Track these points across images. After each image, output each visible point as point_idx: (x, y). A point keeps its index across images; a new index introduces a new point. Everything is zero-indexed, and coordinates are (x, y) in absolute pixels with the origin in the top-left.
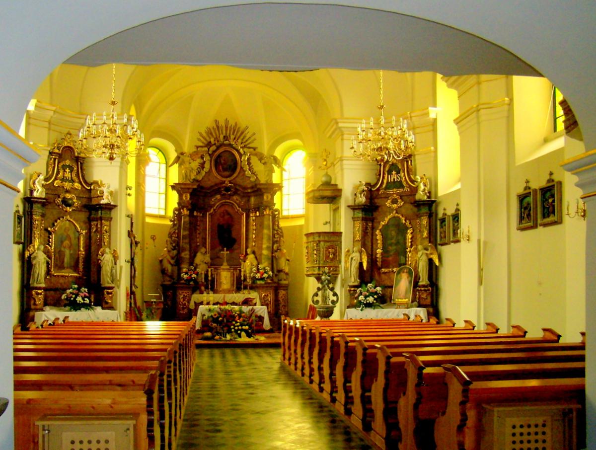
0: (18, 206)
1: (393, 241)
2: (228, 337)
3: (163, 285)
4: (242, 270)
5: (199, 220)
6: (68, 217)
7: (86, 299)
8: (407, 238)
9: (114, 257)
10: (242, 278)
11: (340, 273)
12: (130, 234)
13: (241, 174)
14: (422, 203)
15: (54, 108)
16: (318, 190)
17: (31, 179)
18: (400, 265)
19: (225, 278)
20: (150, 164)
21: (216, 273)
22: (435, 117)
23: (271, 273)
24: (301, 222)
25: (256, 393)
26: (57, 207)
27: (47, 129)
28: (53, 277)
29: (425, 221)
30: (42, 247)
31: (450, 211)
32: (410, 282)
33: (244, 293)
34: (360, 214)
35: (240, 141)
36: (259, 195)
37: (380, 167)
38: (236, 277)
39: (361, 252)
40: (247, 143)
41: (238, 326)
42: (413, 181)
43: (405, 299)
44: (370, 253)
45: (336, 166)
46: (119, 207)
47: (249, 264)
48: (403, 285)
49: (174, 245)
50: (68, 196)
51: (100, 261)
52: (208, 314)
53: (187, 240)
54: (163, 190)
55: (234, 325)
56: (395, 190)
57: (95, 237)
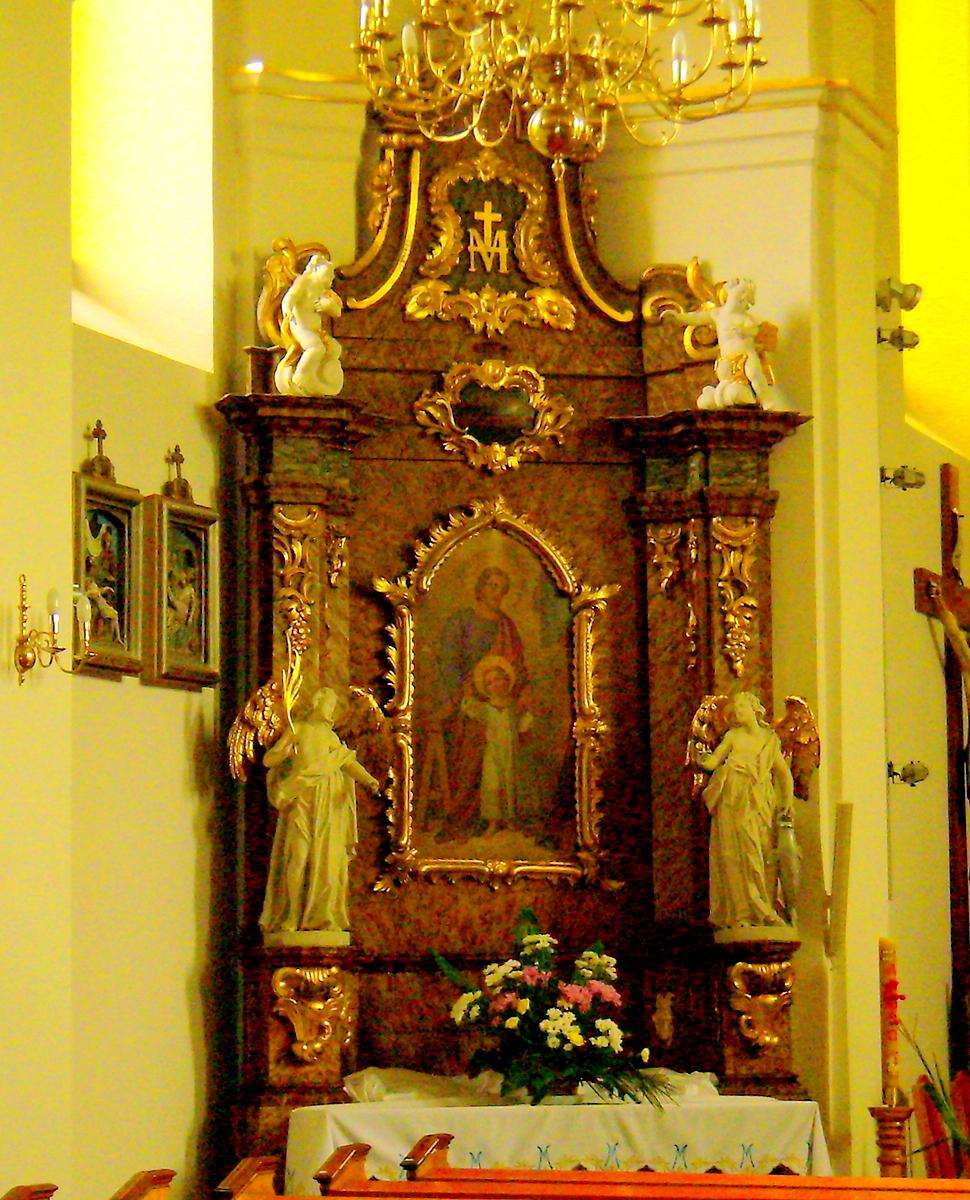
6: (500, 508)
7: (602, 1024)
9: (791, 745)
17: (259, 288)
26: (425, 447)
30: (329, 703)
46: (817, 426)
50: (496, 373)
51: (699, 779)
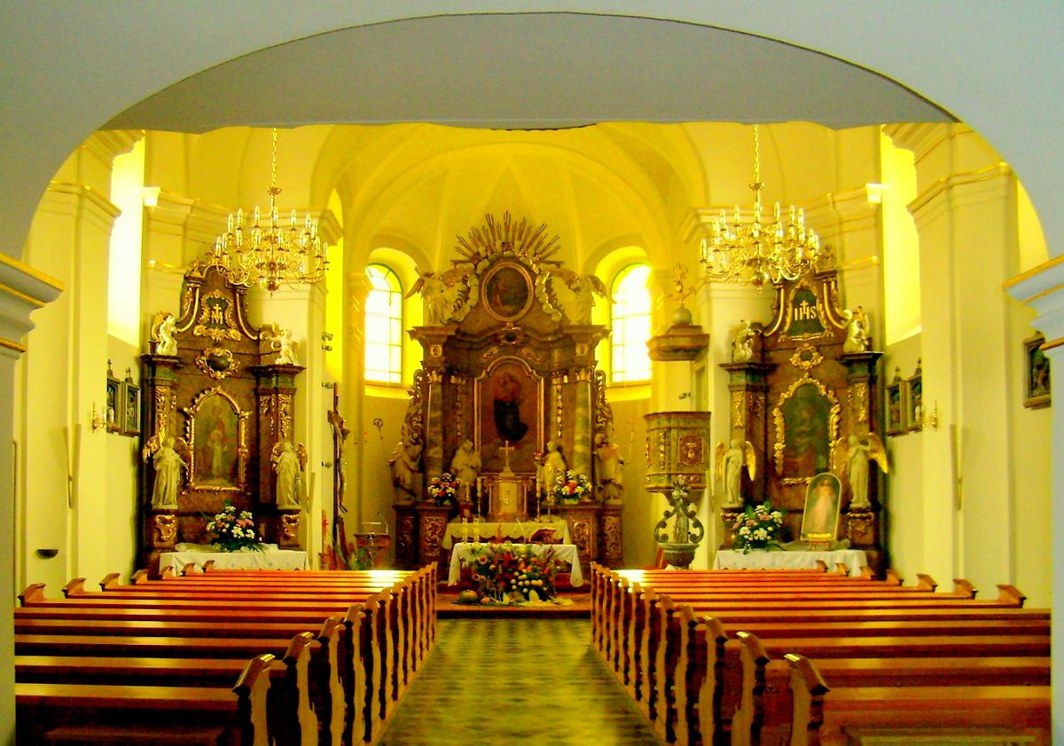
0: (129, 371)
1: (804, 428)
2: (506, 599)
3: (397, 508)
4: (538, 480)
5: (460, 391)
6: (219, 388)
7: (248, 531)
8: (830, 422)
9: (300, 456)
10: (538, 495)
11: (707, 485)
12: (332, 417)
13: (535, 309)
14: (856, 358)
15: (191, 202)
16: (667, 336)
18: (818, 472)
19: (508, 493)
20: (371, 294)
21: (491, 485)
22: (879, 202)
23: (589, 485)
24: (645, 394)
25: (526, 700)
26: (199, 372)
27: (180, 238)
28: (194, 493)
29: (861, 391)
30: (172, 441)
31: (907, 374)
32: (835, 503)
33: (540, 522)
34: (742, 379)
35: (531, 250)
36: (573, 344)
37: (779, 294)
38: (528, 492)
39: (744, 448)
40: (544, 254)
41: (523, 580)
42: (839, 319)
43: (826, 533)
44: (762, 448)
45: (699, 294)
47: (550, 468)
48: (821, 509)
49: (416, 435)
50: (219, 352)
51: (274, 465)
52: (470, 559)
53: (439, 428)
54: (397, 339)
55: (516, 578)
56: (806, 335)
57: (267, 423)
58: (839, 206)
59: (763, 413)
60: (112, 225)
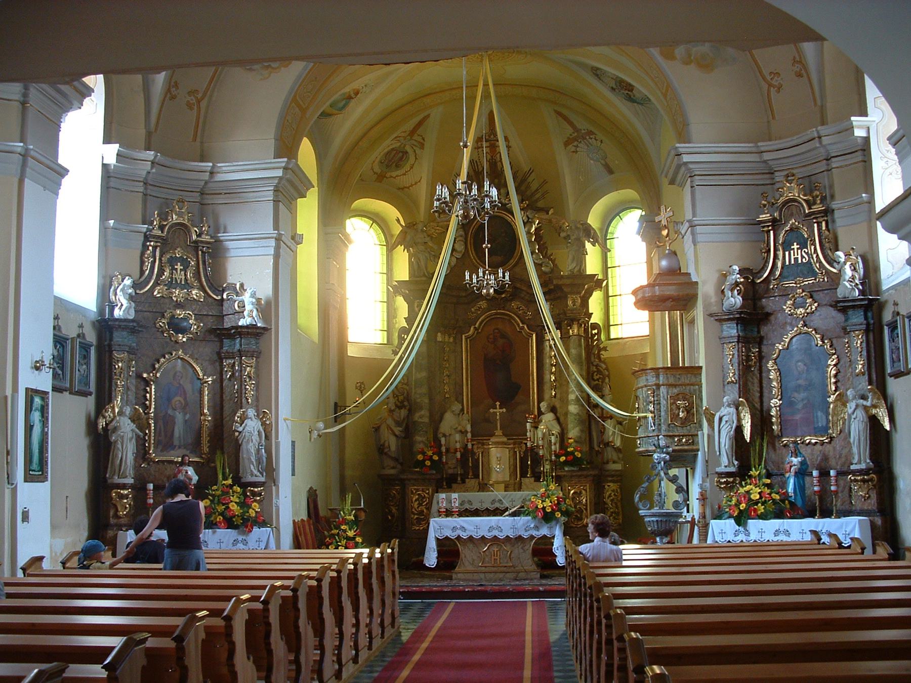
19: (498, 459)
21: (480, 450)
29: (858, 341)
37: (769, 237)
44: (758, 406)
49: (401, 398)
51: (237, 434)
53: (424, 390)
58: (825, 140)
59: (758, 367)
60: (59, 185)
